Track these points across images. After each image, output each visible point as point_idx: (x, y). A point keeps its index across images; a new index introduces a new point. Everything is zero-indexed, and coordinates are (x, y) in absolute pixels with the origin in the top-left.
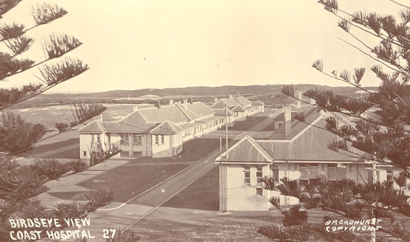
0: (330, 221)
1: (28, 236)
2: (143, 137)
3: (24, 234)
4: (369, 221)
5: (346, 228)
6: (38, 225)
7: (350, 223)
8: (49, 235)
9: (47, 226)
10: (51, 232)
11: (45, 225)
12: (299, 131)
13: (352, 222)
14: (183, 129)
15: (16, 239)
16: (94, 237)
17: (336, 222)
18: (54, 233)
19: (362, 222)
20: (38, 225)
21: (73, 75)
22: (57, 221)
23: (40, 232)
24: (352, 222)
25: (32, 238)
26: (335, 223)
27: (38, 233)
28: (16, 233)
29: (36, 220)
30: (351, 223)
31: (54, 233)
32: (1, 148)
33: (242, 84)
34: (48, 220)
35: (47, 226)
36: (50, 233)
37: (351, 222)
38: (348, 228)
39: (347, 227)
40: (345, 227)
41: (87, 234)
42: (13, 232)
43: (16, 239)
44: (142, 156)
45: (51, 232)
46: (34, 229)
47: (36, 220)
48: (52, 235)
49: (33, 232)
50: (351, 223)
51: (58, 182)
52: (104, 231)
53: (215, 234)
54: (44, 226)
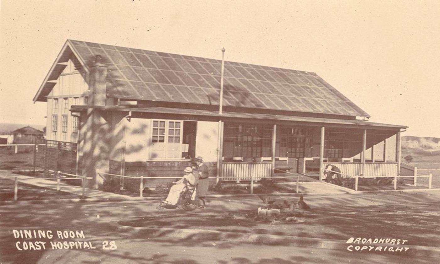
0: (389, 250)
1: (33, 247)
4: (395, 240)
5: (371, 248)
7: (374, 242)
10: (55, 243)
12: (316, 116)
14: (59, 64)
15: (21, 250)
17: (359, 241)
18: (57, 243)
21: (239, 224)
23: (45, 243)
25: (37, 249)
26: (358, 242)
27: (43, 243)
28: (22, 244)
30: (376, 241)
31: (57, 243)
33: (191, 54)
36: (54, 244)
37: (375, 240)
38: (373, 247)
39: (372, 247)
40: (371, 242)
41: (89, 244)
42: (19, 243)
43: (21, 250)
44: (8, 145)
45: (55, 243)
46: (38, 239)
49: (38, 243)
50: (376, 241)
52: (103, 243)
53: (166, 92)
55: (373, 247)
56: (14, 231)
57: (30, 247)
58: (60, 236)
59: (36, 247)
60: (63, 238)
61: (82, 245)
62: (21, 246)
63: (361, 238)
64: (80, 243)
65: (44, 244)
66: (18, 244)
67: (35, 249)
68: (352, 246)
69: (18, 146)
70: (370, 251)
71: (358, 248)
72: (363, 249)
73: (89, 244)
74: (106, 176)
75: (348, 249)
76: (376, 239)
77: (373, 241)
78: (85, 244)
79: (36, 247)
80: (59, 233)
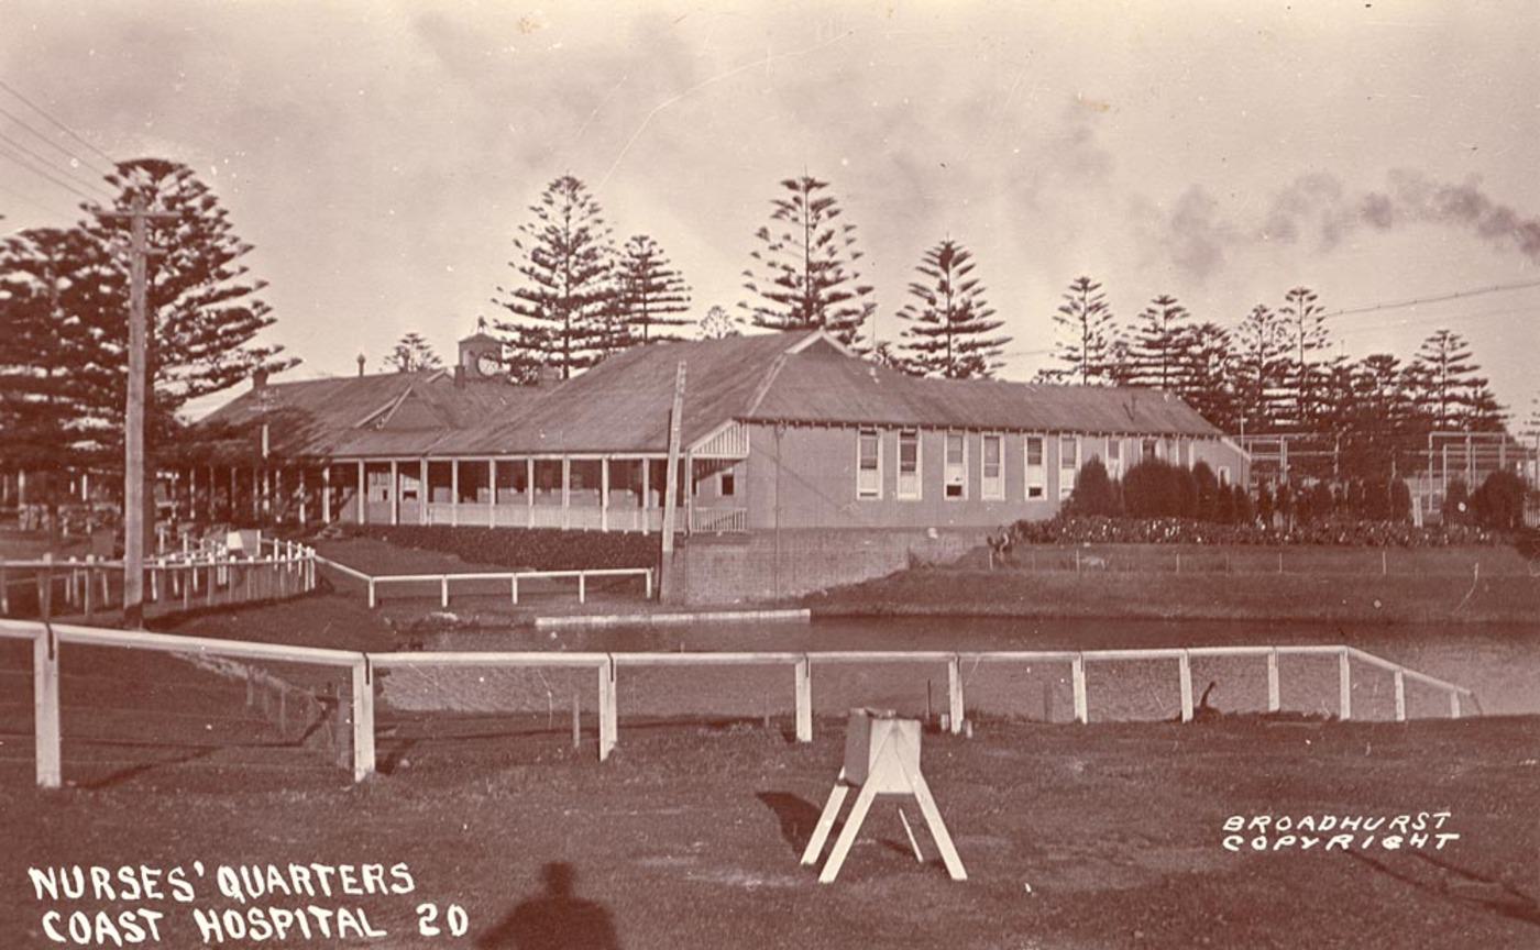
1: (112, 931)
2: (958, 248)
3: (93, 924)
6: (262, 931)
7: (1322, 827)
8: (205, 927)
9: (359, 891)
10: (212, 913)
11: (351, 886)
13: (1329, 822)
15: (59, 938)
16: (383, 933)
19: (1371, 825)
20: (262, 931)
22: (348, 874)
24: (1329, 822)
25: (396, 888)
27: (152, 916)
29: (126, 919)
32: (3, 532)
34: (111, 895)
35: (359, 891)
36: (209, 920)
38: (1316, 840)
39: (1311, 839)
41: (357, 918)
43: (59, 938)
45: (212, 913)
47: (126, 919)
48: (216, 925)
49: (129, 937)
51: (497, 317)
54: (347, 890)
55: (1316, 840)
56: (36, 875)
57: (100, 932)
58: (301, 883)
59: (122, 931)
60: (311, 892)
61: (332, 921)
62: (62, 927)
63: (1337, 817)
64: (322, 914)
65: (156, 921)
66: (53, 922)
67: (119, 941)
68: (125, 895)
69: (1282, 658)
70: (375, 608)
71: (1260, 843)
72: (1282, 846)
73: (357, 918)
74: (863, 880)
75: (1226, 843)
76: (1326, 818)
77: (1318, 822)
78: (346, 919)
79: (122, 931)
80: (300, 874)
